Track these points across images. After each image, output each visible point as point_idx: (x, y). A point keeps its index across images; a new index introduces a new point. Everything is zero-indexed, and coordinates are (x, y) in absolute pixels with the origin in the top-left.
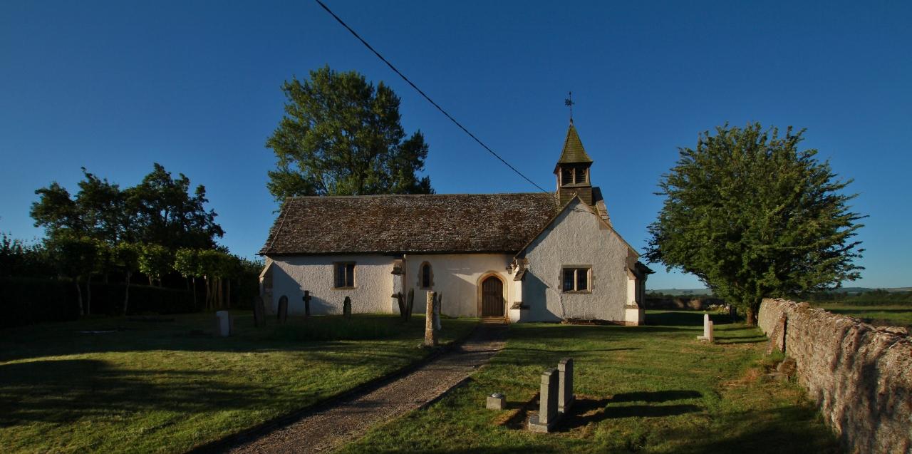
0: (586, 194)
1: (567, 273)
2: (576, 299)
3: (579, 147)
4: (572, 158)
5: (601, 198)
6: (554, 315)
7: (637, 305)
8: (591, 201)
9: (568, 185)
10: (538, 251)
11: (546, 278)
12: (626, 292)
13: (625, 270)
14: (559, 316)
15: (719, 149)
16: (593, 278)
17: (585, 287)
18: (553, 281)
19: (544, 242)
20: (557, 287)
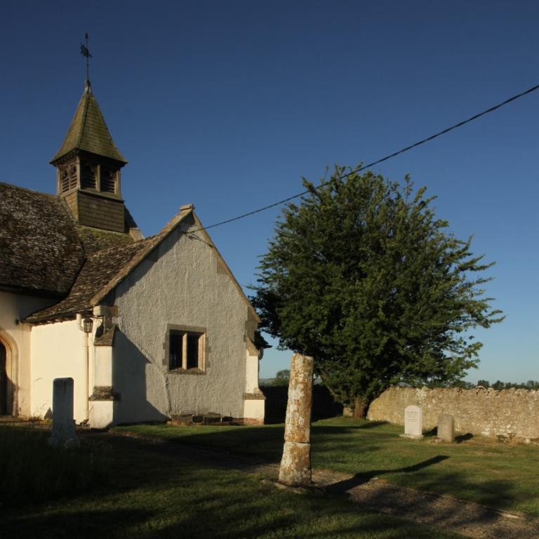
0: (117, 212)
1: (174, 338)
2: (187, 384)
3: (102, 130)
4: (96, 148)
5: (134, 225)
6: (156, 410)
7: (261, 393)
8: (123, 226)
9: (88, 190)
10: (134, 294)
11: (145, 345)
12: (245, 374)
13: (245, 340)
14: (162, 411)
15: (357, 192)
16: (208, 350)
17: (180, 365)
18: (157, 352)
19: (143, 280)
20: (161, 362)
